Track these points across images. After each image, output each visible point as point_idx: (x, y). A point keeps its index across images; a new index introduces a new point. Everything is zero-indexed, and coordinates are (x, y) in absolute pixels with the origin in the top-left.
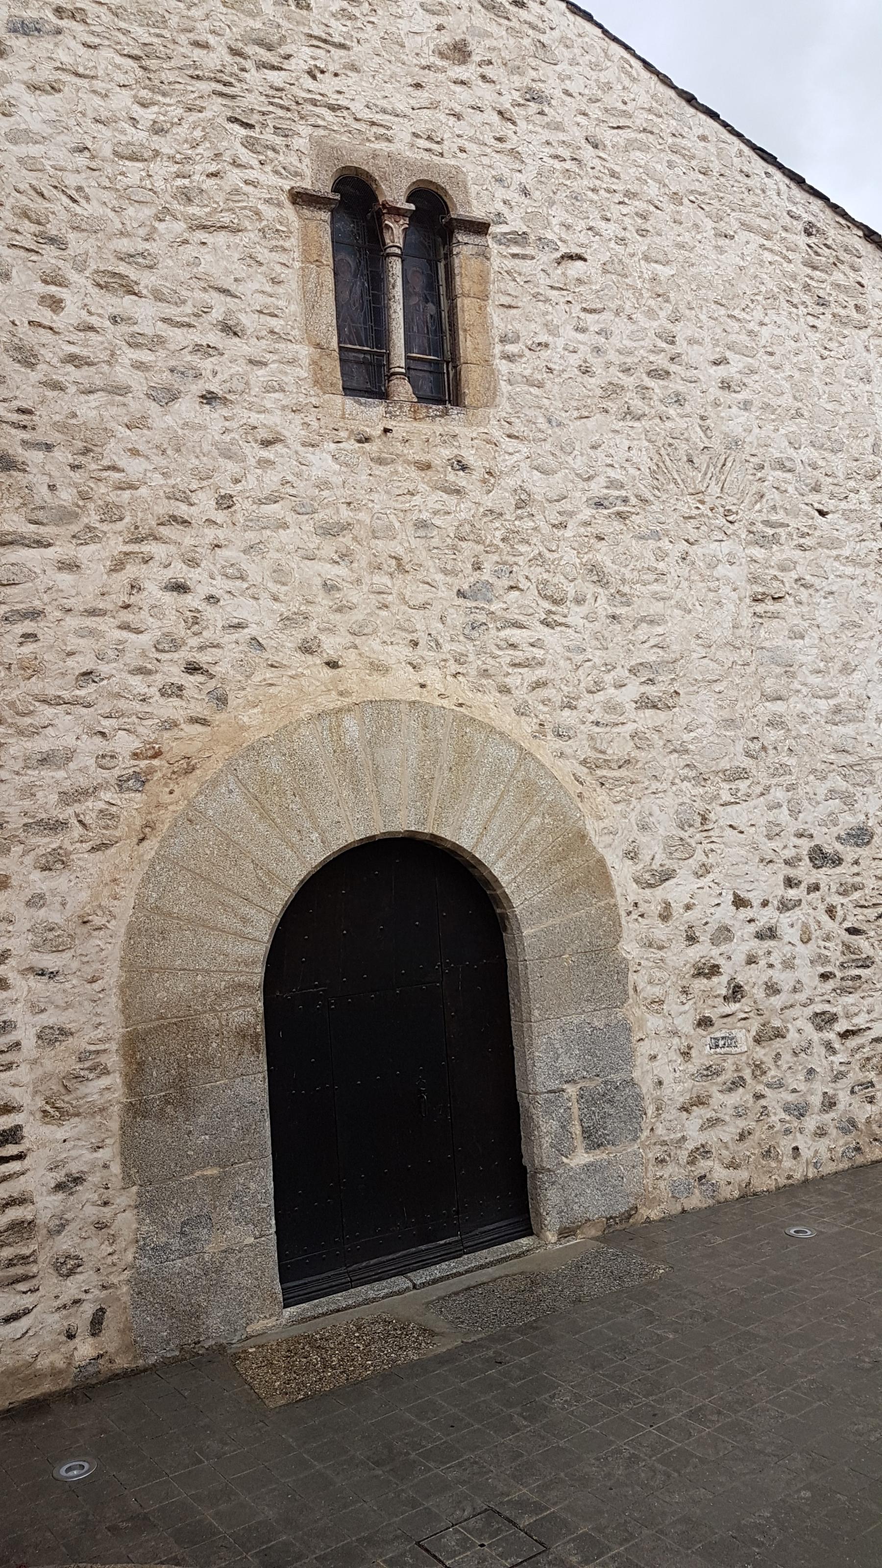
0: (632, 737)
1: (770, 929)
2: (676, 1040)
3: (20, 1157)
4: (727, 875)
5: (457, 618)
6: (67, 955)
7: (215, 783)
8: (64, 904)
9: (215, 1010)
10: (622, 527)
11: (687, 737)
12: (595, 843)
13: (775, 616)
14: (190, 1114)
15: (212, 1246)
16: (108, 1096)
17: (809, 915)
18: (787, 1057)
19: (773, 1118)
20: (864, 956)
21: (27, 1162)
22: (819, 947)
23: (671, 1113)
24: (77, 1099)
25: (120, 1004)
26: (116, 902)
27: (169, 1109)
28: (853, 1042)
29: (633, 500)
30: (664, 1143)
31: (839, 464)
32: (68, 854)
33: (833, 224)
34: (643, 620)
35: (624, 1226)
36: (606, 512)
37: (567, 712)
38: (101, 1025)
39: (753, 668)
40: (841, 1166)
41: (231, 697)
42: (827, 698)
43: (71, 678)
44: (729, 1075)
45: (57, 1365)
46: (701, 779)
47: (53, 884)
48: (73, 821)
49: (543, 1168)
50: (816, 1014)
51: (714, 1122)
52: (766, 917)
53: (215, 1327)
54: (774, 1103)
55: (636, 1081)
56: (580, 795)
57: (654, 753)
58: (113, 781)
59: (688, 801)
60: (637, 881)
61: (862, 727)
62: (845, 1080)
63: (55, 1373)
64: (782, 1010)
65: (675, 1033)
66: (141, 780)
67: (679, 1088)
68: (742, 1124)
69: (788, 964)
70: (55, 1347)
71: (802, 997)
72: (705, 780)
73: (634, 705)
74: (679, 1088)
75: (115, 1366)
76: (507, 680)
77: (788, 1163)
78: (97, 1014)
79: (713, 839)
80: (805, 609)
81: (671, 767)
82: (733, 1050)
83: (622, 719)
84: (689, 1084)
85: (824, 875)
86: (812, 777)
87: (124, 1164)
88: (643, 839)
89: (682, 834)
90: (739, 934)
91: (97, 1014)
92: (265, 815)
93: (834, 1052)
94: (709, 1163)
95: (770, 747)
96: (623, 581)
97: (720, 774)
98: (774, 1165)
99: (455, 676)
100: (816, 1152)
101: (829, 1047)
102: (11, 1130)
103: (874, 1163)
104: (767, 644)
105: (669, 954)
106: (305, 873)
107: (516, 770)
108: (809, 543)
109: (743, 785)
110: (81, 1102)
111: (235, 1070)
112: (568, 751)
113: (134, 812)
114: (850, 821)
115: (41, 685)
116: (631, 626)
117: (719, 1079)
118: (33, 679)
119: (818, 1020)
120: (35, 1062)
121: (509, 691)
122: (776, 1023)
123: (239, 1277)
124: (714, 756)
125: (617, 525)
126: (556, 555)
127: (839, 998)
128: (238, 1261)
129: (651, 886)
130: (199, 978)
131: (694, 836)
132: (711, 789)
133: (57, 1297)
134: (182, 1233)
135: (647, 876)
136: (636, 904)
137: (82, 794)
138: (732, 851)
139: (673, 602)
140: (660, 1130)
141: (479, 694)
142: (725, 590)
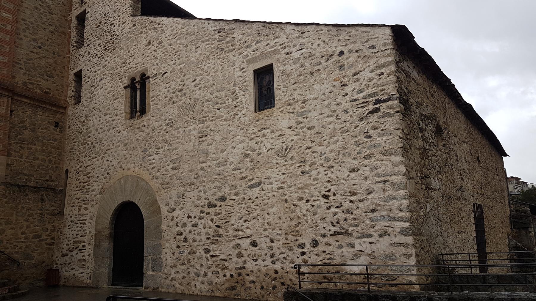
5: (141, 157)
11: (181, 175)
13: (204, 141)
18: (196, 259)
23: (168, 268)
28: (214, 259)
31: (223, 94)
34: (174, 149)
51: (177, 272)
52: (195, 221)
61: (225, 167)
68: (183, 274)
69: (199, 234)
71: (201, 243)
77: (193, 288)
80: (212, 137)
84: (173, 261)
85: (212, 210)
101: (207, 258)
103: (216, 296)
109: (193, 186)
114: (220, 194)
122: (194, 250)
125: (171, 129)
138: (189, 204)
140: (165, 271)
142: (192, 137)
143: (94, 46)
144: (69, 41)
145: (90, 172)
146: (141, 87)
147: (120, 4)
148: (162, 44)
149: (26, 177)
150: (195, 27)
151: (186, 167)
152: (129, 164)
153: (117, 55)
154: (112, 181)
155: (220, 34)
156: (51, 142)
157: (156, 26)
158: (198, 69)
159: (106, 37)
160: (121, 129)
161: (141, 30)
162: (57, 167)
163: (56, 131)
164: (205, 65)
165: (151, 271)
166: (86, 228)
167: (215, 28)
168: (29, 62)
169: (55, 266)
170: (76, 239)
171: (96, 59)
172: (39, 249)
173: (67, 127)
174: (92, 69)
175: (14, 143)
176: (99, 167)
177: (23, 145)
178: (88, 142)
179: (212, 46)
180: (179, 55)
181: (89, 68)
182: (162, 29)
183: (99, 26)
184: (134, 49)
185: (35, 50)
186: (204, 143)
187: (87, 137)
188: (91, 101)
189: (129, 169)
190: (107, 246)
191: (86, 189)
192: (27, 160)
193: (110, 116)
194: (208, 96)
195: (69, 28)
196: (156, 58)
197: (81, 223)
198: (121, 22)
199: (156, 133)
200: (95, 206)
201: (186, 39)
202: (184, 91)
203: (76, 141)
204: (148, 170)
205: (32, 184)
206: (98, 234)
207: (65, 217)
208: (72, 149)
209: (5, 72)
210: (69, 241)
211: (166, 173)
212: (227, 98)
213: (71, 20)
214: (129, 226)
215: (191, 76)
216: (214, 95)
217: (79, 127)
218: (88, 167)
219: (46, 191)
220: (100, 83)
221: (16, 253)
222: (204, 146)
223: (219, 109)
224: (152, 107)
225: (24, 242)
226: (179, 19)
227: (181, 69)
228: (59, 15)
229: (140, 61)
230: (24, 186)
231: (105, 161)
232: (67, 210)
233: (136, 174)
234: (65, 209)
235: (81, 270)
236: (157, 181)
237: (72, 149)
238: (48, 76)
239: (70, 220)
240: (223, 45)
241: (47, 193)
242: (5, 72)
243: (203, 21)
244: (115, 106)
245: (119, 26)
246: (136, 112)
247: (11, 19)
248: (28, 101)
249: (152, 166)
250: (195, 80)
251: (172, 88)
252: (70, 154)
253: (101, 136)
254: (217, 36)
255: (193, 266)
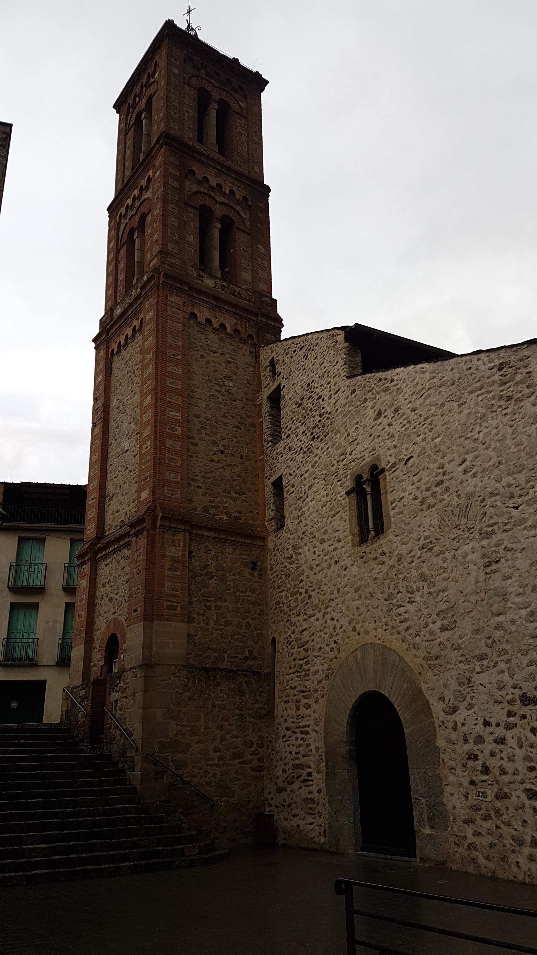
0: (439, 645)
2: (461, 789)
5: (385, 609)
10: (431, 554)
11: (460, 641)
12: (425, 694)
13: (495, 571)
17: (521, 732)
18: (511, 810)
19: (506, 841)
29: (434, 541)
30: (457, 836)
31: (522, 477)
33: (512, 353)
34: (440, 591)
36: (425, 550)
39: (486, 601)
42: (525, 608)
46: (467, 662)
51: (477, 834)
52: (500, 732)
56: (420, 673)
59: (462, 673)
64: (508, 783)
65: (461, 785)
67: (462, 812)
68: (490, 839)
69: (511, 759)
73: (440, 630)
74: (462, 812)
77: (514, 869)
79: (475, 691)
80: (510, 563)
82: (485, 799)
83: (436, 637)
84: (467, 811)
86: (519, 654)
96: (432, 577)
99: (385, 630)
104: (492, 587)
108: (510, 527)
109: (485, 662)
112: (418, 654)
116: (436, 595)
117: (479, 813)
122: (506, 790)
125: (429, 554)
126: (410, 575)
129: (449, 714)
131: (465, 689)
135: (448, 709)
139: (451, 579)
140: (455, 829)
142: (472, 566)
143: (297, 436)
144: (261, 434)
145: (308, 641)
146: (372, 489)
147: (329, 364)
148: (400, 411)
149: (216, 654)
150: (455, 371)
151: (466, 626)
152: (367, 624)
153: (330, 444)
154: (343, 655)
155: (502, 373)
156: (247, 594)
157: (388, 385)
158: (468, 441)
159: (312, 419)
160: (347, 562)
161: (364, 397)
162: (259, 635)
163: (254, 576)
164: (479, 432)
165: (427, 827)
166: (311, 741)
167: (492, 364)
168: (209, 475)
169: (268, 809)
170: (297, 762)
171: (301, 455)
172: (241, 777)
173: (269, 567)
174: (297, 472)
175: (197, 601)
176: (321, 631)
177: (209, 604)
178: (300, 590)
179: (490, 396)
180: (431, 424)
181: (292, 472)
182: (398, 387)
183: (301, 404)
184: (357, 428)
185: (215, 458)
186: (496, 575)
187: (298, 582)
188: (299, 523)
189: (367, 632)
190: (346, 774)
191: (304, 670)
192: (215, 626)
193: (330, 543)
194: (492, 485)
195: (260, 416)
196: (393, 436)
197: (302, 733)
198: (333, 392)
199: (406, 564)
200: (320, 700)
201: (439, 394)
202: (446, 484)
203: (283, 590)
204: (399, 633)
205: (225, 665)
206: (329, 753)
207: (277, 721)
208: (279, 603)
209: (178, 496)
210: (285, 764)
211: (433, 637)
212: (531, 483)
213: (261, 404)
214: (379, 738)
215: (456, 455)
216: (503, 483)
217: (286, 567)
218: (305, 633)
219: (246, 676)
220: (310, 492)
221: (208, 783)
222: (496, 582)
223: (517, 508)
224: (393, 519)
225: (217, 766)
226: (425, 365)
227: (436, 446)
228: (244, 400)
229: (366, 446)
230: (214, 670)
231: (328, 621)
232: (279, 708)
233: (379, 642)
234: (276, 707)
235: (309, 819)
236: (418, 653)
237: (279, 603)
238: (235, 493)
239: (284, 725)
240: (511, 389)
241: (246, 679)
242: (178, 496)
243: (468, 358)
244: (336, 527)
245: (330, 397)
246: (369, 532)
247: (180, 418)
248: (212, 535)
249: (405, 625)
250: (465, 460)
251: (424, 481)
252: (276, 611)
253: (319, 578)
254: (496, 378)
255: (507, 824)
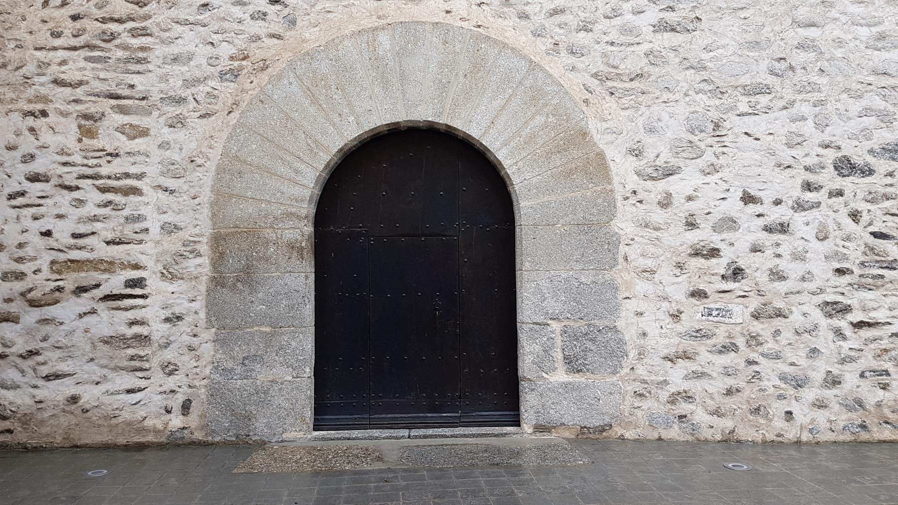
0: (647, 55)
1: (782, 225)
2: (665, 305)
3: (143, 297)
4: (737, 175)
6: (182, 180)
7: (280, 77)
8: (181, 149)
9: (273, 228)
11: (705, 56)
14: (253, 290)
15: (263, 376)
16: (200, 270)
17: (827, 216)
18: (787, 335)
20: (890, 259)
21: (147, 301)
22: (837, 246)
24: (182, 269)
25: (210, 215)
26: (211, 150)
27: (239, 284)
32: (185, 118)
35: (597, 436)
37: (582, 34)
38: (199, 226)
40: (841, 438)
41: (298, 21)
42: (869, 26)
43: (195, 8)
44: (720, 339)
45: (157, 426)
47: (175, 136)
48: (191, 98)
49: (525, 377)
50: (827, 303)
51: (699, 375)
53: (260, 428)
54: (769, 371)
55: (619, 329)
57: (668, 68)
58: (217, 74)
60: (638, 174)
62: (854, 364)
63: (156, 431)
66: (235, 74)
67: (666, 341)
70: (158, 416)
72: (722, 93)
74: (666, 341)
75: (194, 437)
76: (527, 8)
77: (779, 423)
78: (196, 219)
79: (725, 144)
81: (686, 81)
82: (727, 320)
83: (637, 40)
84: (676, 340)
87: (207, 313)
88: (649, 140)
89: (691, 137)
90: (746, 225)
91: (196, 219)
92: (315, 101)
93: (844, 338)
94: (692, 407)
95: (798, 67)
97: (739, 89)
98: (762, 421)
99: (479, 5)
100: (813, 420)
101: (839, 333)
102: (138, 279)
105: (665, 234)
106: (342, 144)
107: (525, 78)
109: (764, 100)
110: (185, 271)
111: (285, 268)
112: (580, 66)
113: (228, 95)
115: (176, 12)
117: (708, 341)
118: (173, 9)
119: (829, 308)
120: (158, 242)
121: (527, 17)
122: (779, 304)
123: (279, 400)
124: (735, 73)
127: (855, 292)
128: (280, 389)
129: (653, 179)
130: (263, 205)
131: (704, 140)
132: (727, 101)
133: (161, 386)
134: (243, 364)
136: (635, 192)
137: (198, 81)
140: (641, 371)
141: (500, 19)
